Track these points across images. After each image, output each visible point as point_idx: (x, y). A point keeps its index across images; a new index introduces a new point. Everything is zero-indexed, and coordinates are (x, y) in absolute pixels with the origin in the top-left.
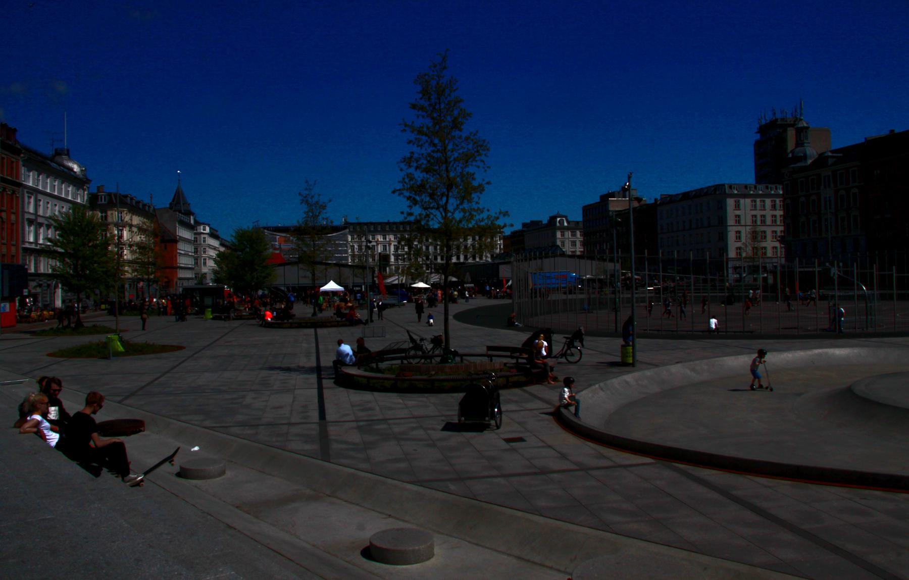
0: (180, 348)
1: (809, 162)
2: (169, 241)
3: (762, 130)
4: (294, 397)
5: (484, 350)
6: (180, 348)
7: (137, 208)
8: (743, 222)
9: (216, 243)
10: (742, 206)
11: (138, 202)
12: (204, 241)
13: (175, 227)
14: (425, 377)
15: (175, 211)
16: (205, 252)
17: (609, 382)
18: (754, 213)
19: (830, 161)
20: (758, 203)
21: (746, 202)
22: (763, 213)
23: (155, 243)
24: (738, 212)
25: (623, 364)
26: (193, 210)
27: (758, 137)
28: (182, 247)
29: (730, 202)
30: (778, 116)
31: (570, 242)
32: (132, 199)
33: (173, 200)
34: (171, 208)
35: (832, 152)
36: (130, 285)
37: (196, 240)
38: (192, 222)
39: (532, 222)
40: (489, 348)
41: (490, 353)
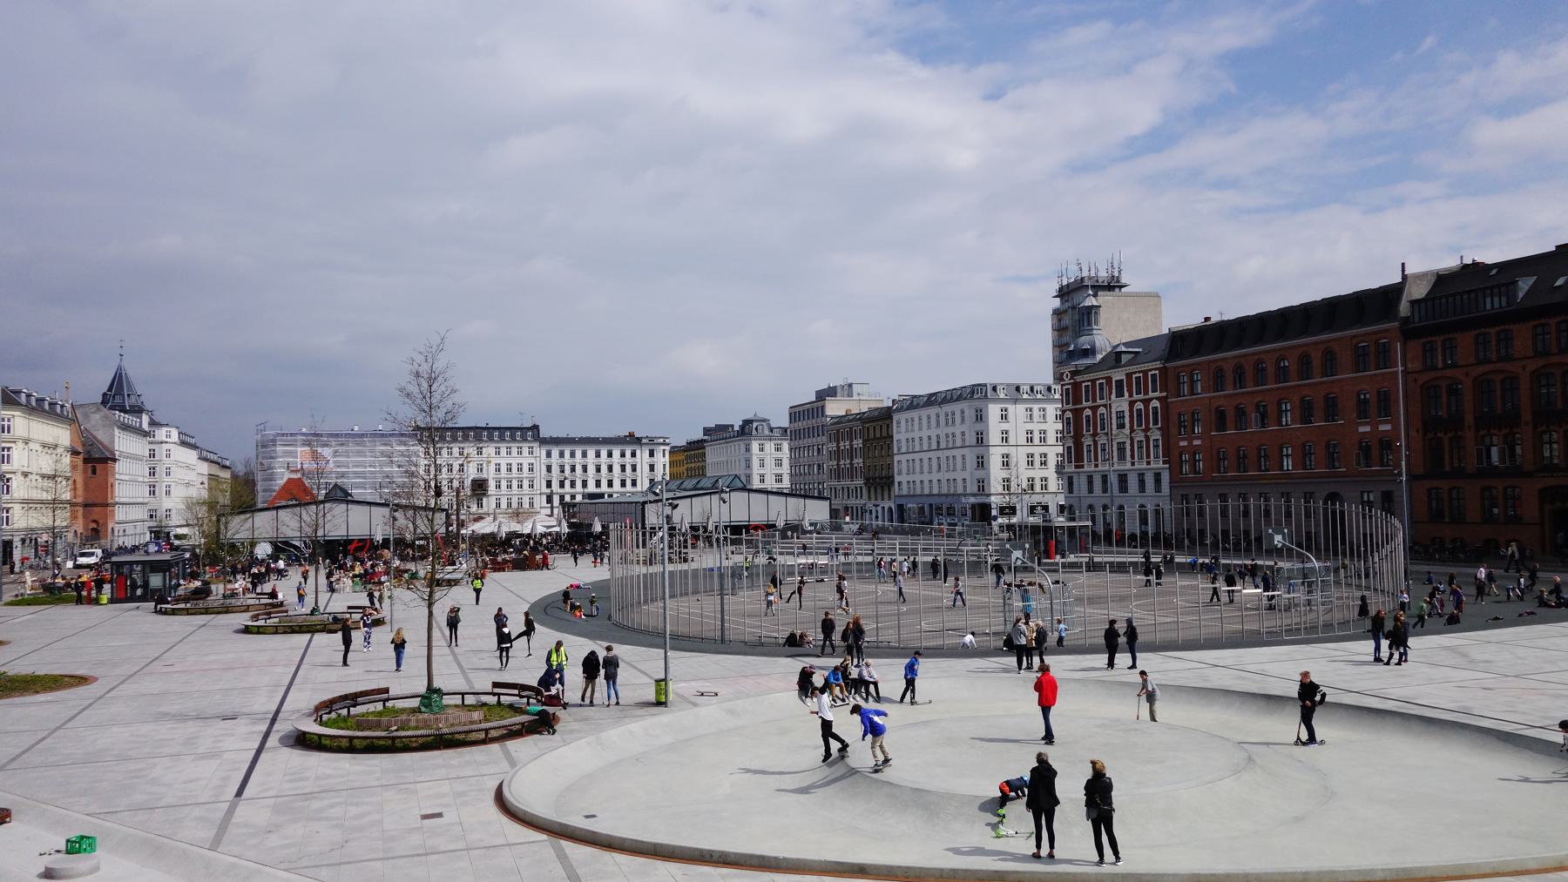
0: (82, 680)
1: (1099, 357)
2: (95, 460)
3: (1064, 293)
4: (880, 481)
5: (489, 688)
6: (82, 680)
7: (42, 409)
8: (1012, 441)
9: (191, 456)
10: (1010, 417)
11: (40, 401)
12: (168, 456)
13: (113, 436)
14: (383, 734)
15: (112, 408)
16: (168, 474)
17: (604, 735)
18: (1030, 426)
19: (1125, 358)
20: (1036, 413)
21: (1017, 411)
22: (1043, 426)
23: (74, 467)
24: (1005, 426)
25: (659, 704)
26: (147, 406)
27: (1057, 303)
28: (121, 468)
29: (994, 411)
30: (1085, 274)
31: (770, 462)
32: (29, 396)
33: (110, 389)
34: (104, 403)
35: (1125, 344)
36: (23, 541)
37: (152, 455)
38: (145, 426)
39: (689, 443)
40: (496, 685)
41: (497, 690)
